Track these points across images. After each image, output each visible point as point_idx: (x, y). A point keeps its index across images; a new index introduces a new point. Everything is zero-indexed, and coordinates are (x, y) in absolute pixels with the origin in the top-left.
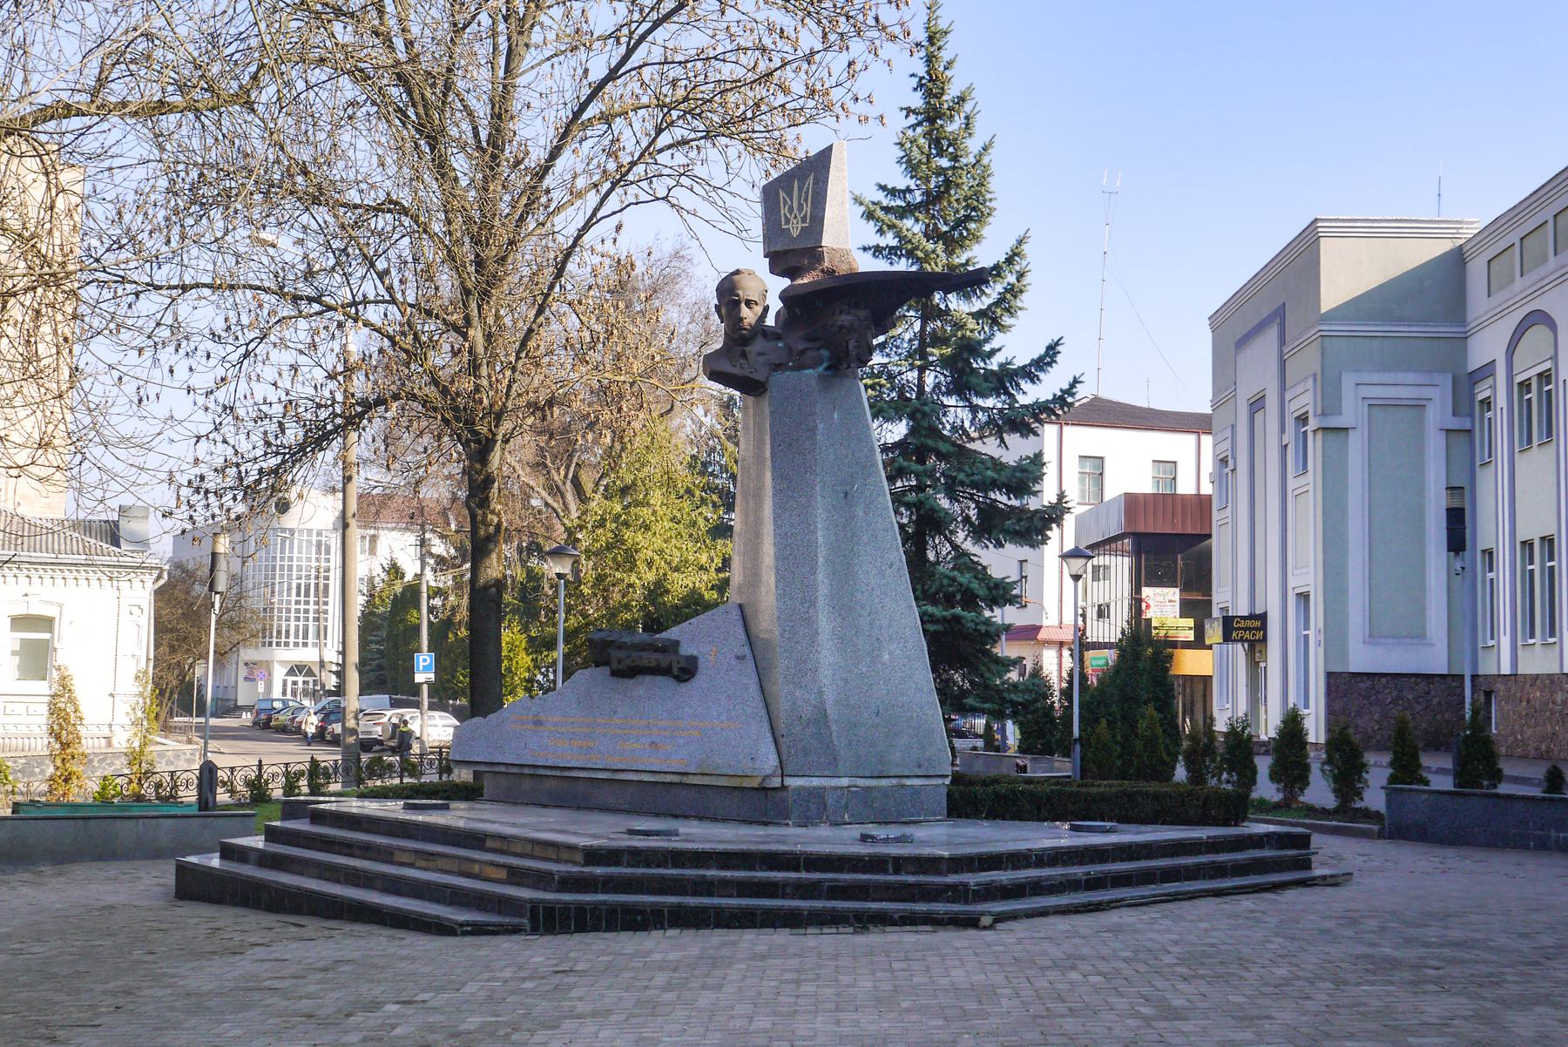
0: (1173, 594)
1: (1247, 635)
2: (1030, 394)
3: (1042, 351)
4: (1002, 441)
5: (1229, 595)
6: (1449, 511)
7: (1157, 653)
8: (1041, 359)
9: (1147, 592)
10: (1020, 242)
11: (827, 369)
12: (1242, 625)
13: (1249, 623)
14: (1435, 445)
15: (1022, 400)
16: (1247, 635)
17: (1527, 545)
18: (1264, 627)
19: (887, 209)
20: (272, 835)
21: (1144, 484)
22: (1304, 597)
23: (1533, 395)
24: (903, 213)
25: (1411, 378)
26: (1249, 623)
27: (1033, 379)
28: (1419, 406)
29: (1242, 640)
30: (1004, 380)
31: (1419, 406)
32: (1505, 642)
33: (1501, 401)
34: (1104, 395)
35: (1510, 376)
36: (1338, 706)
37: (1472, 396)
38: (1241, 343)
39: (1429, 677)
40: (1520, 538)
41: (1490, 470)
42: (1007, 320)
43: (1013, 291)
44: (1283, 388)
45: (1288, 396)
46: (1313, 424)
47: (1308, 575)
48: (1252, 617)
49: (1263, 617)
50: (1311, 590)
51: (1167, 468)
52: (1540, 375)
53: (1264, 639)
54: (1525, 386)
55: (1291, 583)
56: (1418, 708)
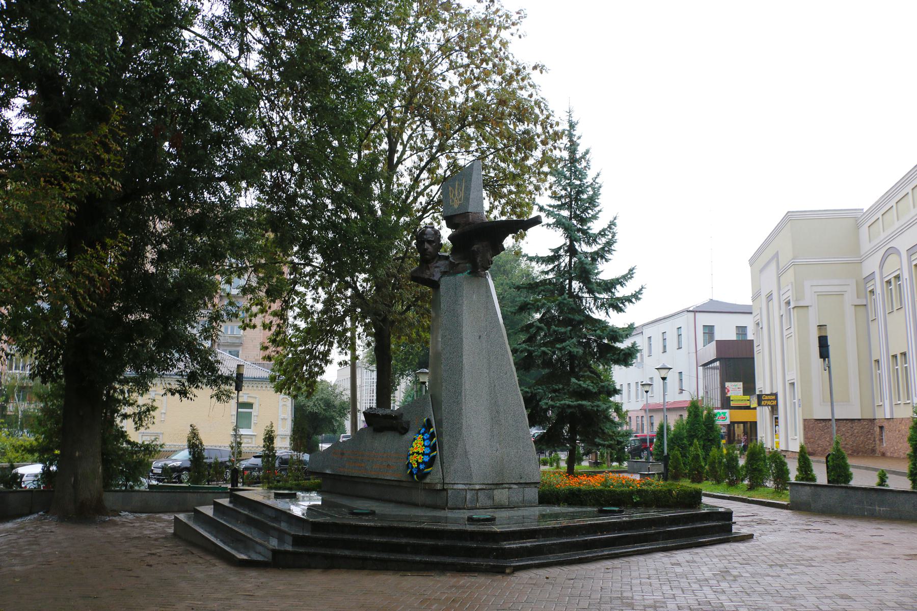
0: (740, 385)
1: (769, 403)
2: (620, 292)
3: (627, 272)
4: (607, 313)
5: (762, 385)
6: (820, 338)
7: (709, 413)
8: (626, 275)
9: (727, 384)
10: (615, 219)
11: (469, 273)
12: (767, 398)
13: (770, 397)
14: (850, 312)
15: (618, 295)
16: (769, 403)
17: (895, 356)
18: (776, 399)
19: (554, 207)
20: (218, 507)
21: (732, 336)
22: (793, 384)
23: (893, 287)
24: (560, 207)
25: (836, 282)
26: (770, 397)
27: (622, 284)
28: (841, 294)
29: (766, 405)
30: (609, 286)
31: (841, 294)
32: (887, 402)
33: (878, 290)
34: (715, 299)
35: (882, 279)
36: (809, 434)
37: (866, 289)
38: (761, 271)
39: (852, 420)
40: (892, 353)
41: (875, 323)
42: (608, 256)
43: (609, 244)
44: (779, 289)
45: (782, 293)
46: (792, 305)
47: (793, 375)
48: (772, 394)
49: (776, 395)
50: (795, 381)
51: (742, 330)
52: (895, 277)
53: (777, 405)
54: (889, 282)
55: (787, 378)
56: (848, 435)
